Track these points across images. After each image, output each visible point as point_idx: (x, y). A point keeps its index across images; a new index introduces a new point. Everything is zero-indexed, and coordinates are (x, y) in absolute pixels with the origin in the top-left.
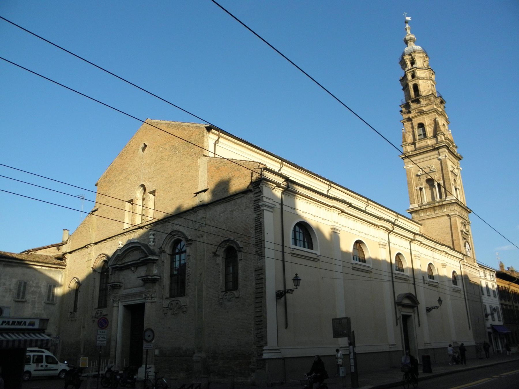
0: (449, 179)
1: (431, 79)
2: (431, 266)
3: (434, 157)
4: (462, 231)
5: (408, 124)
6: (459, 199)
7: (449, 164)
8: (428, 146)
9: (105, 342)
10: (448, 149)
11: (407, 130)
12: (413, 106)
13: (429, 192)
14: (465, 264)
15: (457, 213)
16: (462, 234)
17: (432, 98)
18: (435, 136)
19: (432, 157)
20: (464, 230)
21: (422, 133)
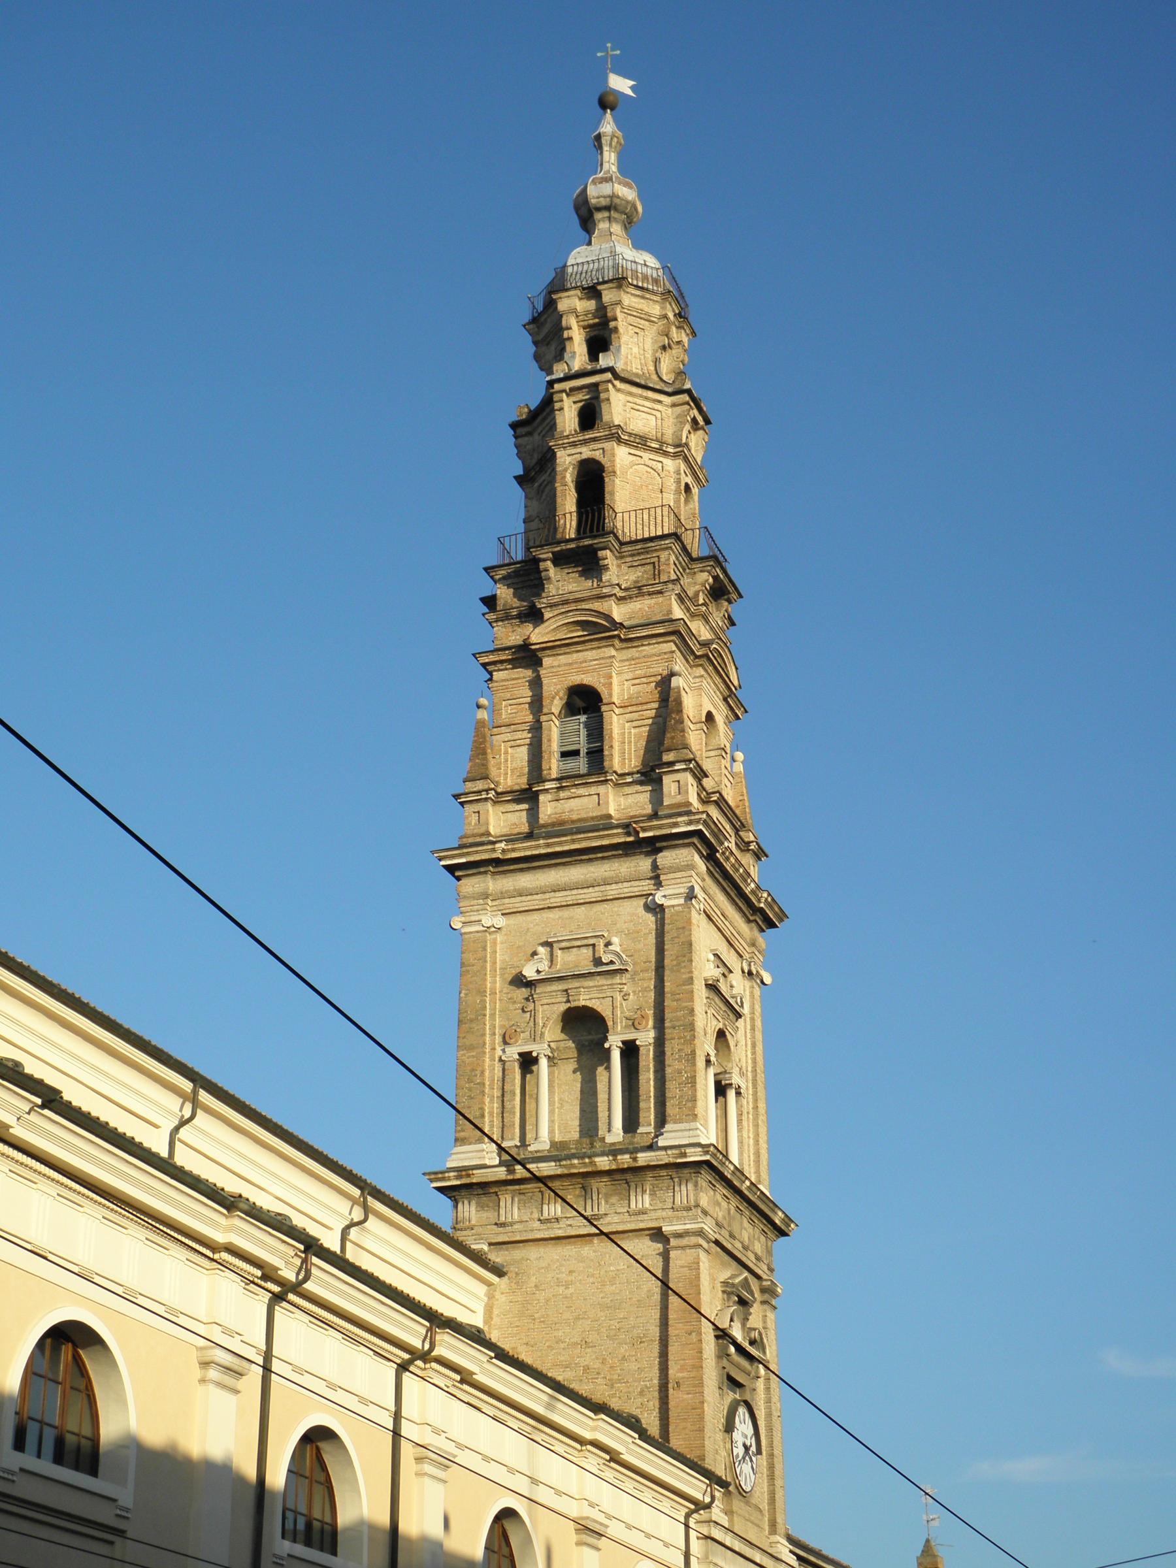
0: (691, 1027)
1: (681, 451)
2: (509, 1526)
3: (626, 889)
4: (722, 1335)
5: (514, 681)
6: (734, 1156)
7: (705, 941)
8: (604, 823)
10: (711, 856)
11: (507, 712)
12: (561, 583)
13: (571, 1082)
14: (717, 1534)
15: (708, 1226)
16: (722, 1354)
17: (669, 559)
18: (651, 774)
19: (613, 890)
20: (737, 1333)
21: (583, 745)
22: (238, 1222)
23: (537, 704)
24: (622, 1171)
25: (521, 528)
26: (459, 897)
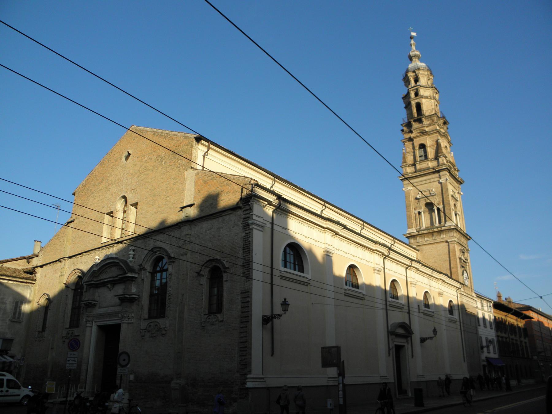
0: (449, 204)
1: (434, 98)
2: (427, 294)
4: (460, 259)
6: (459, 226)
7: (450, 188)
8: (429, 168)
9: (76, 365)
10: (449, 172)
12: (415, 125)
13: (428, 216)
15: (456, 239)
16: (460, 262)
17: (435, 118)
18: (436, 158)
19: (432, 180)
20: (463, 258)
22: (377, 246)
23: (414, 148)
24: (439, 231)
25: (406, 116)
26: (403, 185)
